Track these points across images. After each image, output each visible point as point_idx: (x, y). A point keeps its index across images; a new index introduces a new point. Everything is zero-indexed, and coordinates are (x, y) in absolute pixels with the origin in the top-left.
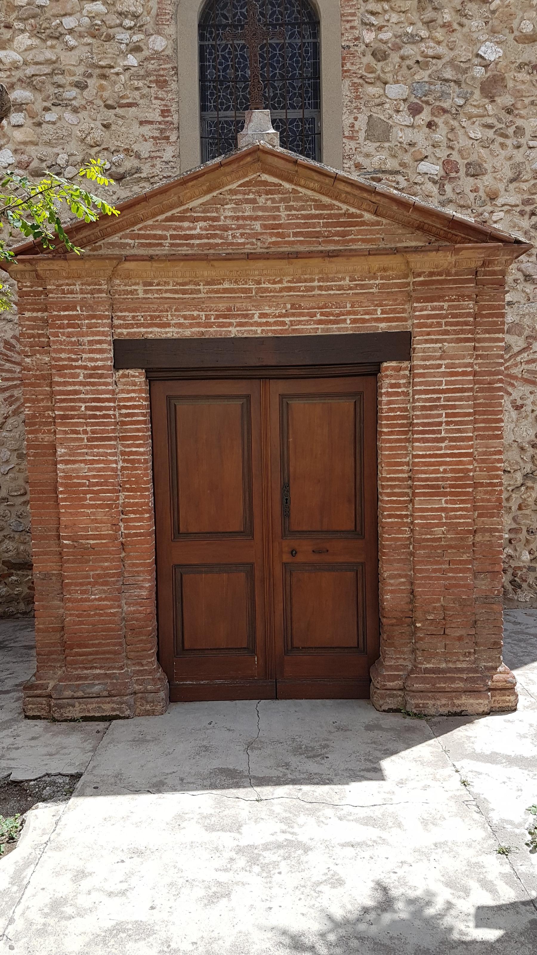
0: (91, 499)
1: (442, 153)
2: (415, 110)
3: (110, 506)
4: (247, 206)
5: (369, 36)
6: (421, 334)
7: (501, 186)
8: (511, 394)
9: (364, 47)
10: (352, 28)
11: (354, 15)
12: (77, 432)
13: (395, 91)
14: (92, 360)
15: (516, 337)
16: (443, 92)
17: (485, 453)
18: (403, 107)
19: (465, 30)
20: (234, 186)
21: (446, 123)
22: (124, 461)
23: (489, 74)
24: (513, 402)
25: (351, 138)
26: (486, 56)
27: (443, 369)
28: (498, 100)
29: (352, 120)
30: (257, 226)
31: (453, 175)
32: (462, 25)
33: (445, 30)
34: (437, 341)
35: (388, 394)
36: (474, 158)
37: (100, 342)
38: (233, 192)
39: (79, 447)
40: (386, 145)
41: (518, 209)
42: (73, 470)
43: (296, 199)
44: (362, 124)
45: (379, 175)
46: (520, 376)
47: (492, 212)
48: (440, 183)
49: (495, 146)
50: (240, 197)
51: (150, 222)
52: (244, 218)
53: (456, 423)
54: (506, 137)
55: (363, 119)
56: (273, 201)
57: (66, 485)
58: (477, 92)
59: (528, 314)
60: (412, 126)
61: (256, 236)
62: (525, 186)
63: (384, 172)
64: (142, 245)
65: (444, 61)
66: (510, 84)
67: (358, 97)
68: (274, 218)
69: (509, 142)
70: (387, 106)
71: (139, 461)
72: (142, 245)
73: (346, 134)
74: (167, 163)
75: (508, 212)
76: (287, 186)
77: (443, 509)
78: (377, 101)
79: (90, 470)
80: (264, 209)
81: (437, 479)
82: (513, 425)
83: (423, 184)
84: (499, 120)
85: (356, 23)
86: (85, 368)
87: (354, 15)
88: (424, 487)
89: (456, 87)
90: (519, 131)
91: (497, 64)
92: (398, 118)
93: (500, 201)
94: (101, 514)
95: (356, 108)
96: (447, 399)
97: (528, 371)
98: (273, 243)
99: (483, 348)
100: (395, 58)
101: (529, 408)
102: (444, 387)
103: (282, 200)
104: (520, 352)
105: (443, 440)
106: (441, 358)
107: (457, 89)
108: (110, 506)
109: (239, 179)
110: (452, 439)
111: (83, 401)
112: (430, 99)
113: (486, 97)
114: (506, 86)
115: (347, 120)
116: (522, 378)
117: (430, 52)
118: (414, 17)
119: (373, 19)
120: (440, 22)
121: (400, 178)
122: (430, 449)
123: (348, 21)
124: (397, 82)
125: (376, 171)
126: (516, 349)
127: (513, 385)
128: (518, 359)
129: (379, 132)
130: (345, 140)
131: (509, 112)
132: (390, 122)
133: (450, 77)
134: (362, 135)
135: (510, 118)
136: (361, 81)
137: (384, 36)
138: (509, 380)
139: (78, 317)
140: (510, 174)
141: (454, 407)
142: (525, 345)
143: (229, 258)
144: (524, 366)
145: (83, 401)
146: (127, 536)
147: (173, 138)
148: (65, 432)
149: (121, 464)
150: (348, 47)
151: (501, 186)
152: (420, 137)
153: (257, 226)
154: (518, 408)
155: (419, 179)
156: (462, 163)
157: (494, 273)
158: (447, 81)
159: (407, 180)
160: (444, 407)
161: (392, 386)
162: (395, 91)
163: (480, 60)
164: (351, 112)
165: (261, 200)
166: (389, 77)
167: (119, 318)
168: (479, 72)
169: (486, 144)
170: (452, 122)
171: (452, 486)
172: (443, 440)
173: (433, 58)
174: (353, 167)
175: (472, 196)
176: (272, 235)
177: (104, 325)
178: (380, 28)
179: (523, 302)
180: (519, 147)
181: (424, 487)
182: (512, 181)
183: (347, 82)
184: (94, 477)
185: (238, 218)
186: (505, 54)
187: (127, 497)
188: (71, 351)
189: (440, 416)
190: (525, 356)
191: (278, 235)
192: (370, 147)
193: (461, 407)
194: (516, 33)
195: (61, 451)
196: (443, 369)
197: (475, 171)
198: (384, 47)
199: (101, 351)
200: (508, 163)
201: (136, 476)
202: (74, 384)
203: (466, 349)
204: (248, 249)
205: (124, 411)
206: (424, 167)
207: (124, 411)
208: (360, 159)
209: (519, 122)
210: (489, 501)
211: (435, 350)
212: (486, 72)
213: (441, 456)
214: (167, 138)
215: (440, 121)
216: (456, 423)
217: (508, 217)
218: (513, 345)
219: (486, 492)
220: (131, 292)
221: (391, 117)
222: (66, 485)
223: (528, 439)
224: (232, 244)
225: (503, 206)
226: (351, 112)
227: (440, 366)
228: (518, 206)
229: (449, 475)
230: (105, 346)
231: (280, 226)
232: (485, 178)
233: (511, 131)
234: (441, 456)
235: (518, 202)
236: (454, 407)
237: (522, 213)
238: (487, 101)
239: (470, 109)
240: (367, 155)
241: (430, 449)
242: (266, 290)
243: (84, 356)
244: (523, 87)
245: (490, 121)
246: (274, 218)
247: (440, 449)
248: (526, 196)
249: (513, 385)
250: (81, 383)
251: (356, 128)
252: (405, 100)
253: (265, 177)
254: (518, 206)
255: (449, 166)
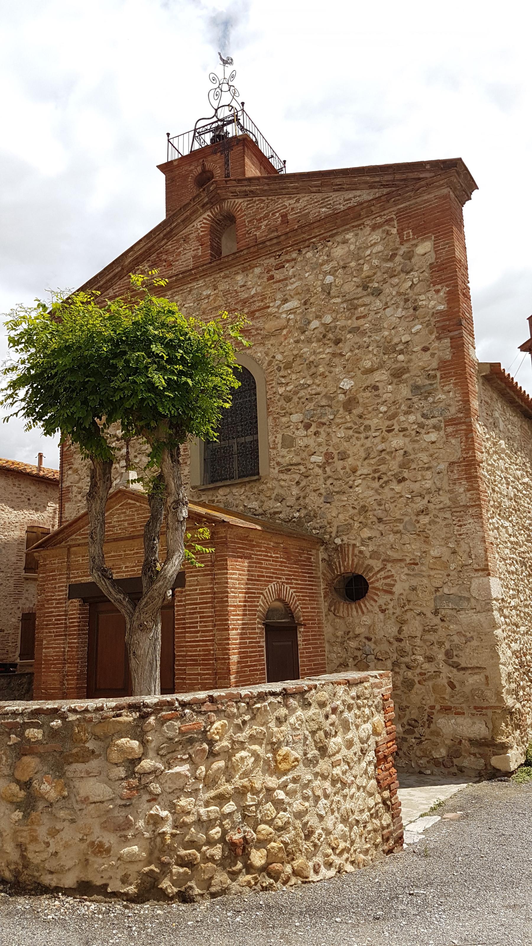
0: (53, 668)
1: (323, 449)
2: (307, 427)
3: (59, 672)
4: (122, 515)
5: (281, 390)
6: (188, 572)
7: (359, 464)
8: (376, 601)
9: (278, 396)
10: (272, 387)
11: (272, 380)
12: (50, 632)
13: (296, 418)
14: (59, 595)
15: (376, 561)
16: (321, 413)
17: (220, 640)
18: (300, 426)
19: (333, 374)
20: (118, 507)
21: (324, 431)
22: (69, 647)
23: (347, 397)
24: (380, 607)
25: (274, 448)
26: (344, 387)
27: (198, 591)
28: (354, 411)
29: (274, 438)
30: (126, 524)
31: (330, 461)
32: (330, 373)
33: (321, 377)
34: (195, 576)
35: (177, 606)
36: (342, 449)
37: (62, 586)
38: (117, 509)
39: (51, 640)
40: (293, 449)
41: (370, 476)
42: (48, 652)
43: (142, 509)
44: (279, 440)
45: (289, 467)
46: (381, 588)
47: (354, 481)
48: (322, 466)
49: (354, 440)
50: (120, 511)
51: (86, 527)
52: (121, 521)
53: (205, 622)
54: (359, 433)
55: (279, 436)
56: (132, 511)
57: (45, 660)
58: (341, 409)
59: (382, 544)
60: (307, 436)
61: (125, 529)
62: (372, 462)
63: (291, 465)
64: (83, 538)
65: (322, 395)
66: (361, 400)
67: (276, 425)
68: (133, 519)
69: (362, 436)
70: (291, 427)
71: (74, 647)
72: (83, 538)
73: (271, 446)
74: (186, 476)
75: (364, 479)
76: (138, 504)
77: (199, 674)
78: (286, 425)
79: (54, 652)
80: (128, 516)
81: (195, 656)
82: (382, 624)
83: (313, 469)
84: (355, 424)
85: (273, 385)
86: (56, 599)
87: (272, 380)
88: (190, 660)
89: (329, 409)
90: (368, 428)
91: (350, 391)
92: (297, 433)
93: (359, 473)
94: (56, 676)
95: (276, 431)
96: (200, 608)
97: (386, 584)
98: (132, 531)
99: (219, 579)
100: (295, 399)
101: (391, 611)
102: (199, 601)
103: (136, 511)
104: (379, 571)
105: (198, 632)
106: (197, 585)
107: (330, 410)
108: (59, 672)
109: (119, 503)
110: (203, 631)
111: (54, 616)
112: (315, 419)
113: (347, 411)
114: (358, 402)
115: (271, 438)
116: (383, 589)
117: (313, 392)
118: (306, 373)
119: (283, 380)
120: (318, 373)
121: (301, 467)
122: (193, 637)
123: (270, 384)
124: (297, 413)
125: (288, 465)
126: (377, 569)
127: (377, 595)
128: (378, 576)
129: (288, 442)
130: (270, 450)
131: (360, 417)
132: (294, 436)
133: (325, 404)
134: (279, 445)
135: (361, 421)
136: (278, 416)
137: (288, 389)
138: (374, 591)
139: (55, 575)
140: (364, 455)
141: (203, 612)
142: (381, 566)
143: (115, 540)
144: (383, 581)
145: (54, 616)
146: (68, 689)
147: (188, 463)
148: (47, 633)
149: (67, 649)
150: (271, 398)
151: (359, 464)
152: (311, 441)
153: (126, 524)
154: (383, 611)
155: (312, 466)
156: (335, 452)
157: (222, 538)
158: (323, 406)
159: (306, 468)
160: (199, 613)
161: (179, 601)
162: (296, 418)
163: (341, 390)
164: (273, 434)
165: (128, 512)
166: (293, 410)
167: (72, 574)
168: (341, 397)
169: (348, 439)
170: (328, 430)
171: (203, 660)
172: (198, 632)
173: (316, 395)
174: (276, 465)
175: (342, 472)
176: (131, 527)
177: (64, 578)
178: (287, 384)
179: (378, 536)
180: (367, 438)
181: (190, 660)
182: (365, 459)
183: (271, 418)
184: (55, 656)
185: (119, 521)
186: (355, 383)
187: (69, 667)
188: (52, 592)
189: (197, 618)
190: (382, 574)
191: (134, 527)
192: (284, 452)
193: (206, 612)
194: (362, 369)
195: (45, 642)
196: (198, 591)
197: (343, 456)
198: (289, 394)
199: (62, 591)
200: (363, 448)
201: (72, 655)
202: (51, 608)
203: (207, 579)
204: (122, 535)
205: (71, 621)
206: (313, 459)
207: (71, 621)
208: (279, 459)
209: (367, 422)
210: (223, 669)
211: (194, 581)
212: (345, 396)
213: (198, 641)
214: (186, 463)
215: (321, 430)
216: (205, 622)
217: (365, 482)
218: (374, 566)
219: (222, 664)
220: (77, 561)
221: (294, 433)
222: (45, 660)
223: (393, 635)
224: (116, 534)
225: (361, 475)
226: (273, 434)
227: (196, 590)
228: (370, 474)
229: (201, 653)
230: (64, 588)
231: (134, 523)
232: (349, 459)
233: (362, 428)
234: (198, 641)
235: (369, 472)
236: (203, 612)
237: (374, 479)
238: (347, 413)
239: (338, 421)
240: (283, 457)
241: (193, 637)
242: (128, 554)
243: (57, 594)
244: (367, 401)
245: (349, 425)
246: (133, 519)
247: (197, 637)
248: (374, 468)
249: (377, 595)
250: (55, 608)
251: (276, 442)
252: (302, 422)
253: (130, 501)
254: (370, 474)
255: (328, 456)
